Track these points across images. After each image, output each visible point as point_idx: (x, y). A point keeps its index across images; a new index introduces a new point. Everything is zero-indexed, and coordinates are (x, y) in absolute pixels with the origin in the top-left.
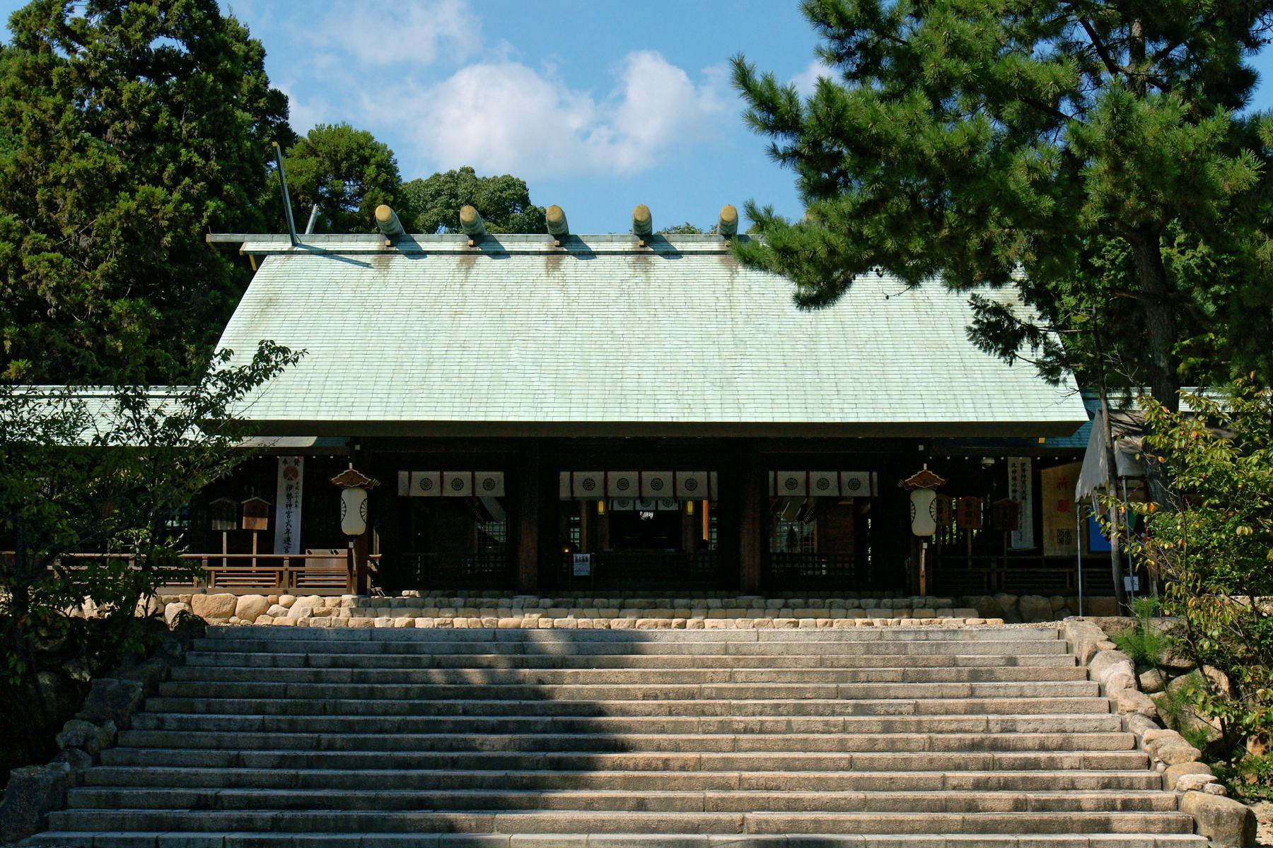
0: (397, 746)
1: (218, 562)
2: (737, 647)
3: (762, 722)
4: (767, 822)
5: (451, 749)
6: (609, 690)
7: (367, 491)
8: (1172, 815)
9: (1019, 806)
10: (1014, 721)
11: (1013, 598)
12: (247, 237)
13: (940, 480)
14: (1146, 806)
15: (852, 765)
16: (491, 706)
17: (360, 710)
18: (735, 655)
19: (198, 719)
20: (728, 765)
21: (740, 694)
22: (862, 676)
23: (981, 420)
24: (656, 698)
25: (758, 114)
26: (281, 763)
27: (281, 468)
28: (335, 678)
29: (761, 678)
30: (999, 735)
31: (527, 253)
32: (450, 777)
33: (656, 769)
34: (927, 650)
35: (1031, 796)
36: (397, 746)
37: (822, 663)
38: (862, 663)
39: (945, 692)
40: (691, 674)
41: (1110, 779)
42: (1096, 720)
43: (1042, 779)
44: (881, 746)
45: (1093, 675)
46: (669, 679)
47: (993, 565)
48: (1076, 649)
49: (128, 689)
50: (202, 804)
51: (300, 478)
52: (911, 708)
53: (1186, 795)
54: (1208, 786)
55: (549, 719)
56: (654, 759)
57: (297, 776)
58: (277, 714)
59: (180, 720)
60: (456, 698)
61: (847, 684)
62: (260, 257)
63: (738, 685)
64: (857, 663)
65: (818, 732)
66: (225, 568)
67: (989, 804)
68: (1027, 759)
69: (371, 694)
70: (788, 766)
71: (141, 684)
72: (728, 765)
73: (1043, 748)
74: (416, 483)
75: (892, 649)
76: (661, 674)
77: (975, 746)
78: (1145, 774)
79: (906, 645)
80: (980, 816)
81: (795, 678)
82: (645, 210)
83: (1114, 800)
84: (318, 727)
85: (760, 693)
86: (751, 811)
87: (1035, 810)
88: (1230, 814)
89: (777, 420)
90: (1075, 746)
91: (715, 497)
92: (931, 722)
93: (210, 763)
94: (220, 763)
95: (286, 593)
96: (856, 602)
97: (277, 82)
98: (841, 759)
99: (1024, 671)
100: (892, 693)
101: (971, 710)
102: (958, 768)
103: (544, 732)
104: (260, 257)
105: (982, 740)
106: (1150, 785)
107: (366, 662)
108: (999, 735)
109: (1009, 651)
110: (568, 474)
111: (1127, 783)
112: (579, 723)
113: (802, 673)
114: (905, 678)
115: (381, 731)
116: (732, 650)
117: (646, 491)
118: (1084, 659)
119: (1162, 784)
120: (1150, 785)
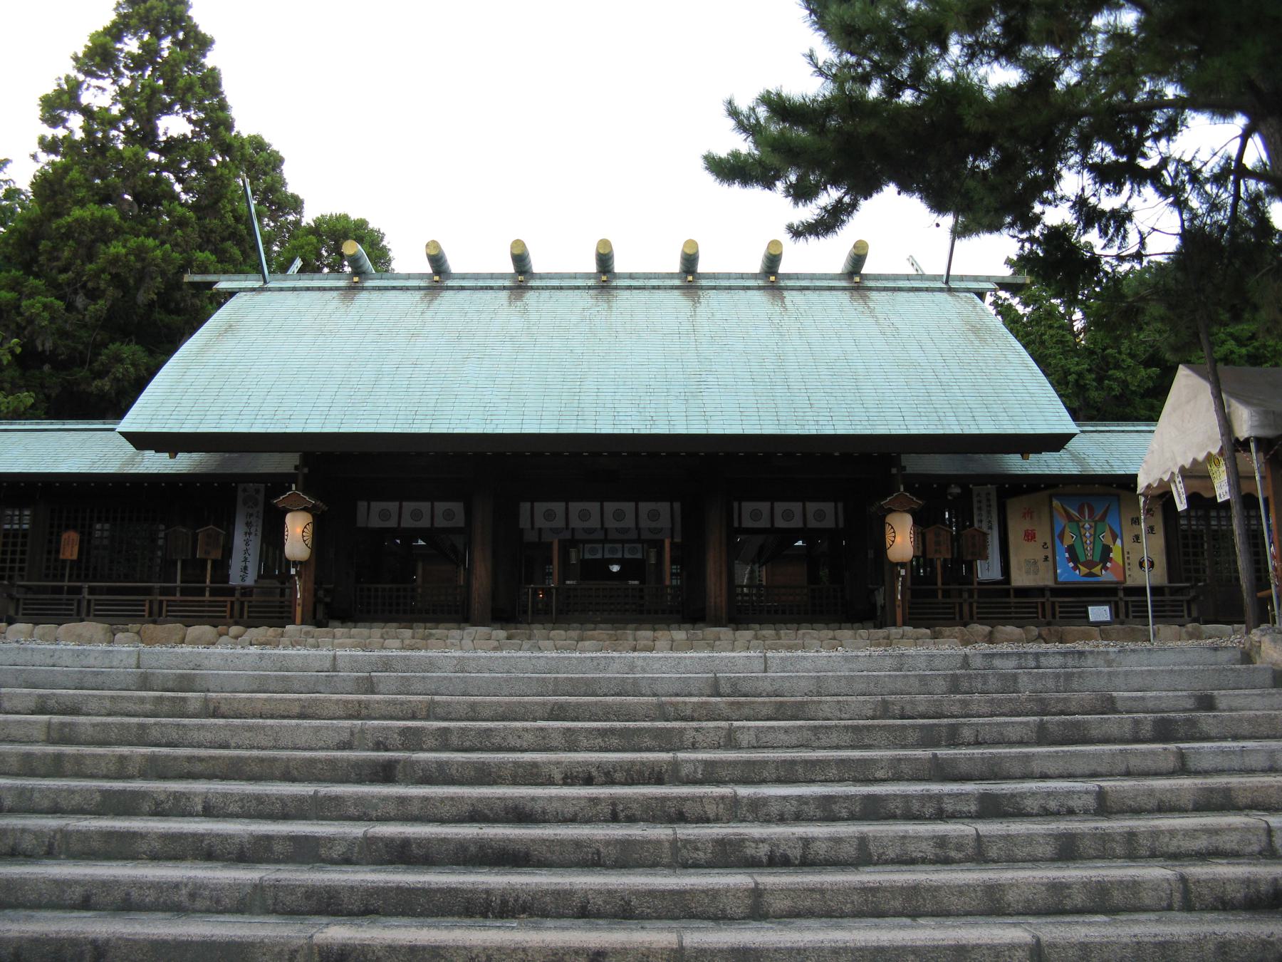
1: (170, 591)
2: (734, 683)
7: (314, 516)
11: (988, 629)
12: (222, 277)
13: (918, 503)
18: (732, 697)
22: (967, 733)
23: (967, 431)
24: (589, 781)
27: (240, 496)
31: (491, 288)
34: (1051, 684)
37: (884, 710)
38: (956, 709)
39: (1135, 763)
44: (1079, 899)
46: (615, 741)
47: (966, 595)
52: (1091, 802)
62: (231, 294)
64: (946, 709)
66: (178, 597)
74: (376, 514)
76: (603, 733)
81: (847, 738)
82: (605, 243)
89: (746, 432)
95: (236, 624)
96: (831, 633)
99: (1250, 720)
100: (1036, 767)
107: (93, 705)
110: (528, 505)
113: (856, 729)
114: (1043, 737)
116: (725, 688)
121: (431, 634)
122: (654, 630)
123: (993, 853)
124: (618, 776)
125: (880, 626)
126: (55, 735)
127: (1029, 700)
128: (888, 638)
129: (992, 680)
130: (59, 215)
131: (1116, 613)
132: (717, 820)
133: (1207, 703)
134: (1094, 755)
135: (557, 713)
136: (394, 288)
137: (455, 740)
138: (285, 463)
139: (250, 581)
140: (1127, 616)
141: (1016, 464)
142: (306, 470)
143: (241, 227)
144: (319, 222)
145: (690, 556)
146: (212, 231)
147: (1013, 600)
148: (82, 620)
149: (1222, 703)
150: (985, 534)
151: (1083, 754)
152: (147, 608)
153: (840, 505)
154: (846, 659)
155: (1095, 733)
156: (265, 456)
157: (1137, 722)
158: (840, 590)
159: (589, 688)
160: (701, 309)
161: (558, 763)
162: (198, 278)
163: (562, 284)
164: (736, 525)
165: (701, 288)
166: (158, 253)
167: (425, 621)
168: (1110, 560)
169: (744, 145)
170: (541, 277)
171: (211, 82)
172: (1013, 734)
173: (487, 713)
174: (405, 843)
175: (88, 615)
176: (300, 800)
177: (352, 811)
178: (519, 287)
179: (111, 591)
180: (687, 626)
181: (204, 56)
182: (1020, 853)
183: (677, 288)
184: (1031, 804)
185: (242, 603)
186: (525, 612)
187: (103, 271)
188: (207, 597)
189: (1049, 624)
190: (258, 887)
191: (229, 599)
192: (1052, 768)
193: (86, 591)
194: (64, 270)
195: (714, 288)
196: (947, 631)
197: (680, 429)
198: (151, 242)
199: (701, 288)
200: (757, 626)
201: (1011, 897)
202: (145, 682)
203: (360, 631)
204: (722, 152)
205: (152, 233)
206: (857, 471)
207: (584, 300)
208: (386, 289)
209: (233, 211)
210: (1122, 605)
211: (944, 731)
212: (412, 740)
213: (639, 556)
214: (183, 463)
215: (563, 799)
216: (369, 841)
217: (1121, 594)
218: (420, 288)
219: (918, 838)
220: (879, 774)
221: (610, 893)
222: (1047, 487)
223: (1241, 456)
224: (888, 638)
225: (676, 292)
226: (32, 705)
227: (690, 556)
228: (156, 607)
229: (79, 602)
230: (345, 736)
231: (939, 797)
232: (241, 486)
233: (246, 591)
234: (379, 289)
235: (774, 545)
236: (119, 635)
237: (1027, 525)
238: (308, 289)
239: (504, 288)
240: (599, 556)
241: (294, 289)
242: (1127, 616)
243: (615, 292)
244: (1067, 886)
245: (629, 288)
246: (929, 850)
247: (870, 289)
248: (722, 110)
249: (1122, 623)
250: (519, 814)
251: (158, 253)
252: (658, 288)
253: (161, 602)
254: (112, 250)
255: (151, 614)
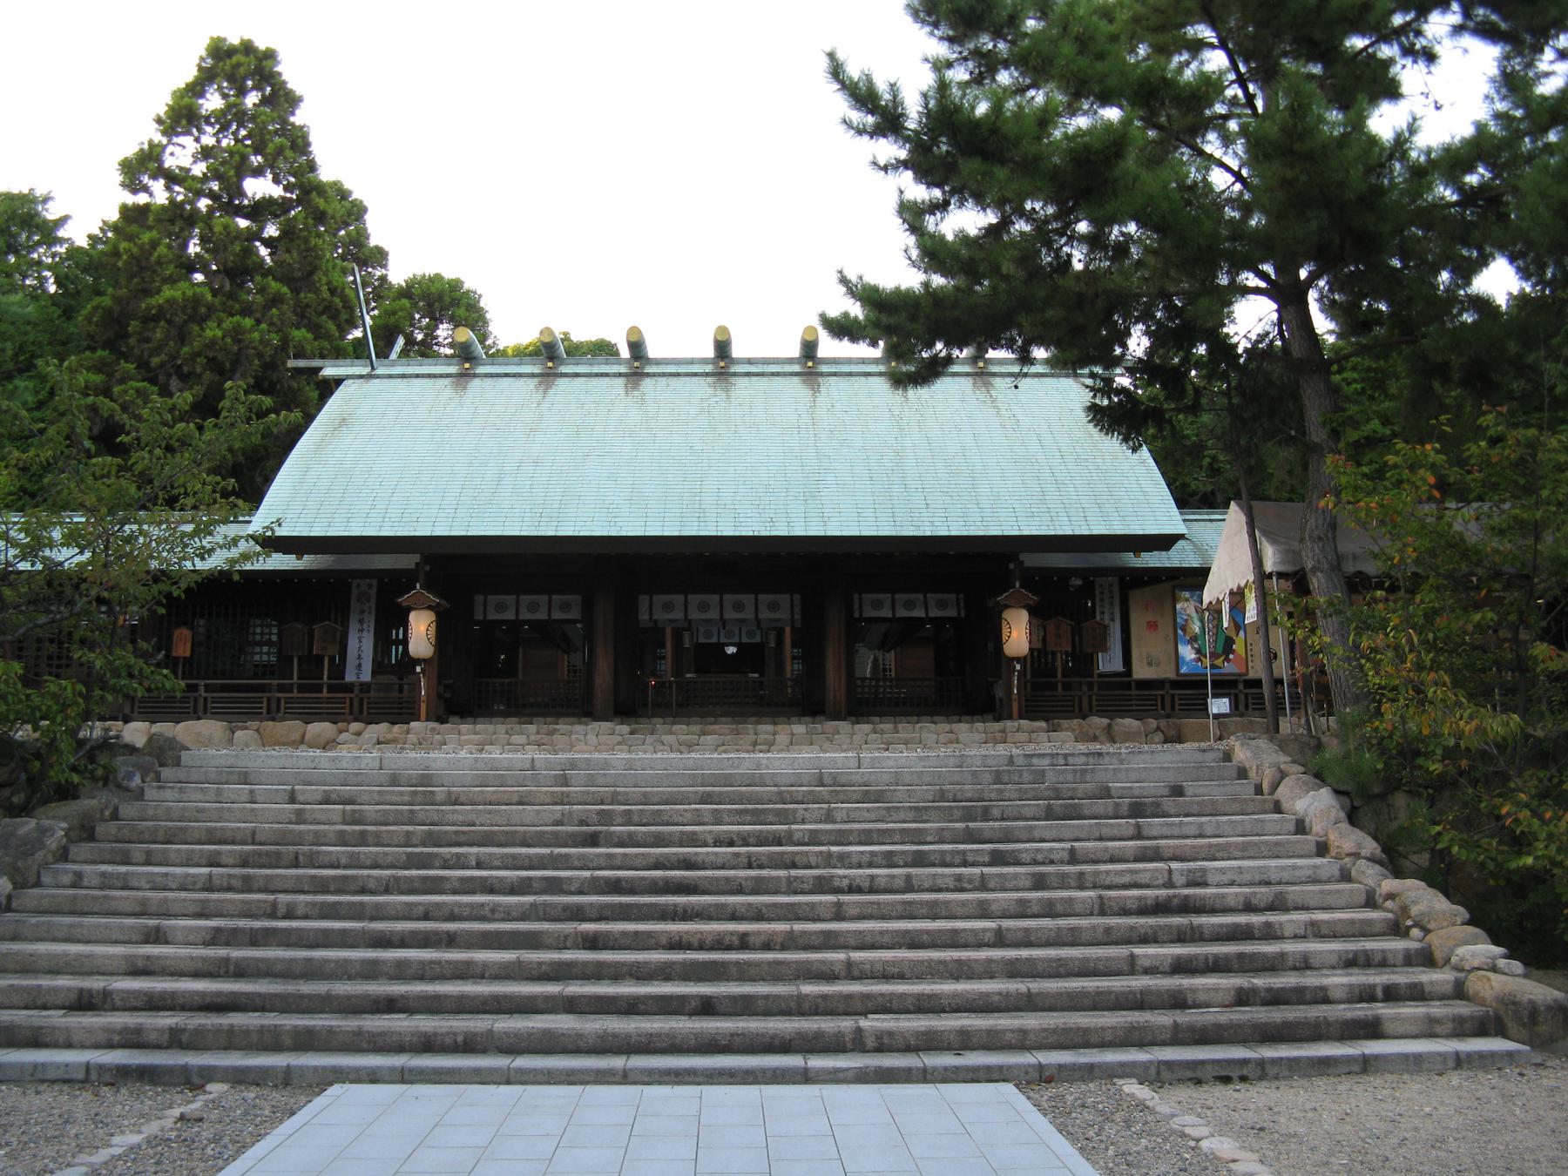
0: (379, 914)
1: (289, 689)
2: (834, 777)
3: (873, 877)
4: (890, 1034)
5: (452, 918)
6: (670, 834)
7: (437, 614)
8: (1463, 1009)
9: (1243, 998)
10: (1204, 871)
11: (1106, 721)
12: (327, 362)
14: (1417, 994)
15: (1000, 940)
16: (514, 856)
17: (343, 862)
18: (831, 786)
19: (126, 874)
20: (829, 941)
21: (841, 838)
22: (996, 812)
24: (731, 844)
25: (856, 116)
26: (216, 938)
27: (355, 592)
28: (323, 818)
29: (864, 817)
30: (1186, 891)
31: (607, 375)
32: (439, 963)
33: (729, 948)
34: (1070, 777)
35: (1259, 982)
36: (379, 914)
37: (942, 796)
38: (993, 796)
39: (1105, 832)
40: (778, 813)
41: (1356, 953)
42: (1308, 867)
43: (1264, 955)
44: (1036, 909)
45: (1285, 805)
47: (1085, 688)
48: (1252, 774)
49: (43, 832)
50: (85, 1003)
51: (373, 603)
52: (1065, 855)
53: (1472, 977)
54: (1502, 963)
55: (587, 874)
56: (726, 933)
57: (227, 960)
58: (234, 866)
59: (103, 874)
60: (471, 845)
61: (971, 809)
62: (338, 381)
63: (837, 826)
64: (986, 795)
65: (948, 890)
66: (295, 694)
67: (1202, 997)
68: (1236, 925)
69: (363, 839)
70: (913, 942)
71: (64, 825)
72: (829, 941)
73: (1249, 908)
74: (500, 608)
75: (1026, 777)
76: (740, 812)
77: (1160, 908)
78: (1397, 945)
79: (1043, 772)
80: (1185, 1017)
81: (911, 815)
82: (723, 330)
83: (1373, 987)
84: (280, 886)
85: (866, 838)
86: (865, 1014)
87: (1266, 1003)
88: (1549, 1008)
90: (1290, 904)
91: (798, 625)
92: (1097, 873)
93: (122, 938)
94: (134, 938)
95: (356, 720)
96: (947, 727)
97: (377, 236)
98: (984, 930)
99: (1198, 803)
100: (1037, 834)
101: (1141, 857)
102: (1145, 940)
103: (580, 892)
104: (338, 381)
105: (1169, 898)
106: (1410, 960)
108: (1186, 891)
109: (1172, 778)
110: (647, 597)
111: (1378, 958)
112: (627, 880)
113: (916, 808)
114: (1050, 815)
115: (363, 891)
116: (827, 780)
117: (728, 620)
118: (1265, 786)
119: (1427, 959)
120: (1410, 960)
121: (555, 730)
122: (775, 724)
123: (992, 885)
124: (751, 840)
125: (998, 719)
126: (348, 819)
127: (1047, 789)
128: (1003, 731)
129: (1025, 775)
130: (147, 293)
131: (1235, 705)
132: (817, 867)
133: (1178, 791)
134: (1078, 826)
135: (706, 799)
136: (507, 375)
137: (636, 818)
138: (407, 561)
139: (366, 676)
140: (1247, 707)
141: (1133, 560)
142: (428, 568)
143: (337, 300)
144: (411, 284)
145: (810, 640)
146: (307, 306)
147: (1134, 692)
148: (199, 718)
149: (1189, 791)
150: (1106, 627)
151: (1070, 826)
152: (265, 705)
153: (797, 597)
154: (920, 758)
155: (1087, 812)
156: (378, 557)
157: (1117, 805)
158: (959, 682)
159: (727, 781)
160: (821, 399)
161: (710, 832)
162: (302, 363)
163: (678, 370)
164: (857, 615)
165: (822, 374)
166: (256, 335)
167: (545, 715)
168: (1233, 652)
169: (856, 310)
170: (658, 362)
171: (299, 142)
172: (1028, 812)
173: (656, 799)
174: (618, 880)
175: (205, 712)
176: (542, 856)
177: (576, 863)
178: (635, 374)
179: (225, 688)
180: (808, 719)
181: (293, 114)
182: (1009, 885)
183: (797, 374)
184: (1025, 857)
185: (361, 700)
186: (645, 705)
187: (198, 354)
188: (325, 694)
189: (1168, 716)
190: (534, 905)
191: (348, 695)
192: (1047, 835)
193: (202, 689)
194: (157, 351)
195: (835, 374)
196: (1065, 723)
197: (799, 531)
198: (248, 322)
199: (822, 374)
200: (877, 719)
201: (994, 907)
202: (394, 780)
203: (484, 728)
204: (834, 313)
205: (246, 311)
206: (974, 571)
207: (702, 387)
208: (498, 375)
209: (329, 283)
210: (1242, 697)
211: (980, 812)
212: (606, 818)
213: (757, 640)
214: (306, 562)
215: (716, 854)
216: (594, 879)
217: (1241, 686)
218: (533, 375)
219: (944, 876)
220: (929, 839)
221: (750, 904)
222: (1169, 579)
223: (1266, 583)
224: (1003, 731)
225: (796, 379)
226: (319, 798)
227: (810, 640)
228: (274, 705)
229: (196, 699)
230: (558, 816)
231: (964, 852)
232: (355, 582)
233: (365, 687)
234: (491, 376)
235: (902, 634)
236: (239, 733)
237: (1149, 617)
238: (418, 376)
239: (620, 375)
240: (714, 640)
241: (403, 376)
242: (1247, 707)
243: (733, 380)
244: (1029, 901)
245: (748, 374)
246: (951, 883)
247: (994, 375)
248: (835, 277)
249: (1241, 716)
250: (688, 864)
251: (256, 335)
252: (778, 374)
253: (279, 699)
254: (209, 333)
255: (269, 711)
